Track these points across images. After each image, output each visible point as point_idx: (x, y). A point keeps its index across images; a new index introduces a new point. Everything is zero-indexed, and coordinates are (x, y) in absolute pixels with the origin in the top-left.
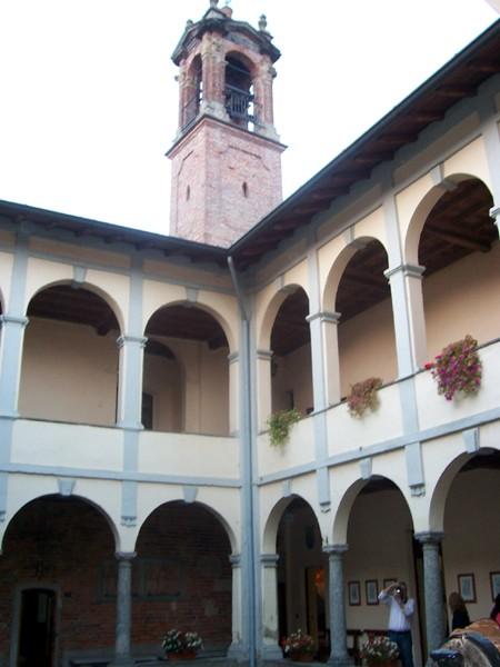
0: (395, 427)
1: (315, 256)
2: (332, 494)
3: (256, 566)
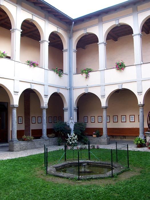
0: (137, 73)
3: (73, 112)
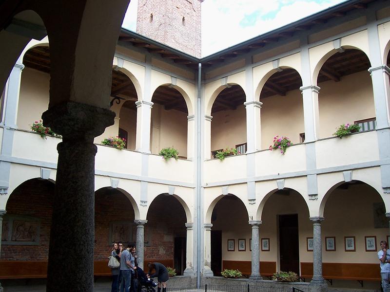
1: (251, 72)
3: (202, 229)
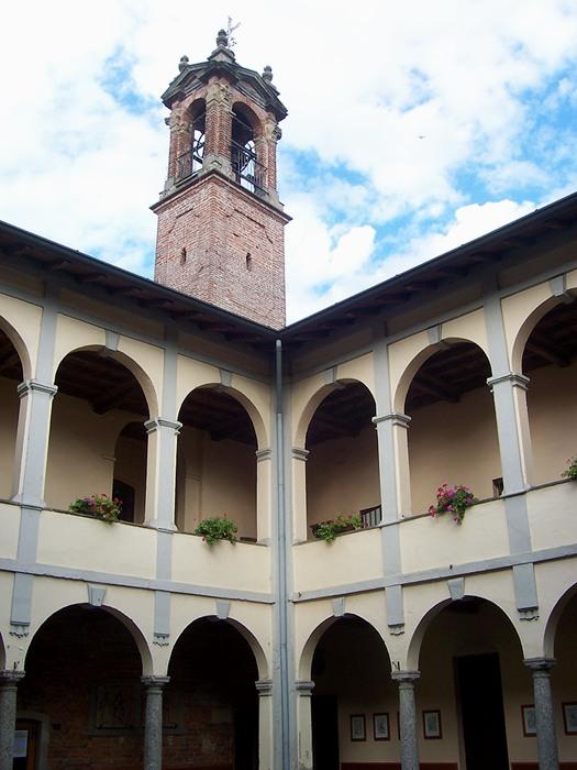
2: (405, 615)
3: (291, 695)
